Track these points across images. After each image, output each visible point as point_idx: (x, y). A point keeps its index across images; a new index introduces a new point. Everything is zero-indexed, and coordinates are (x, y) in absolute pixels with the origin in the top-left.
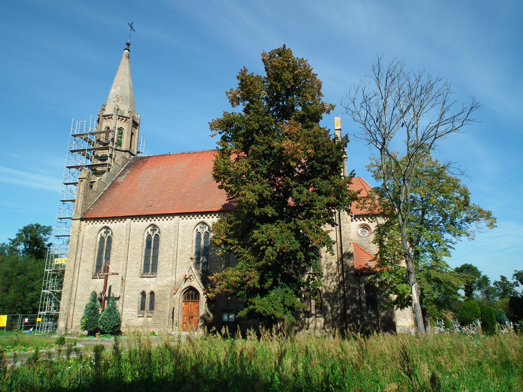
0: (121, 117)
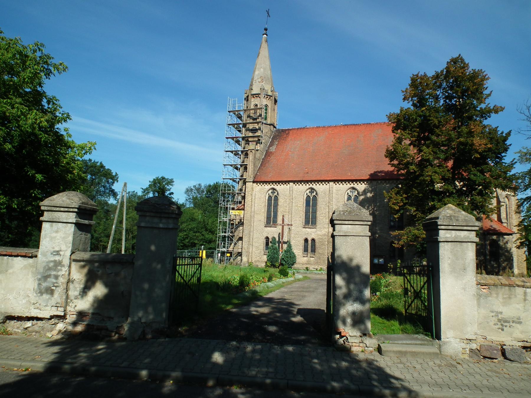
0: (268, 96)
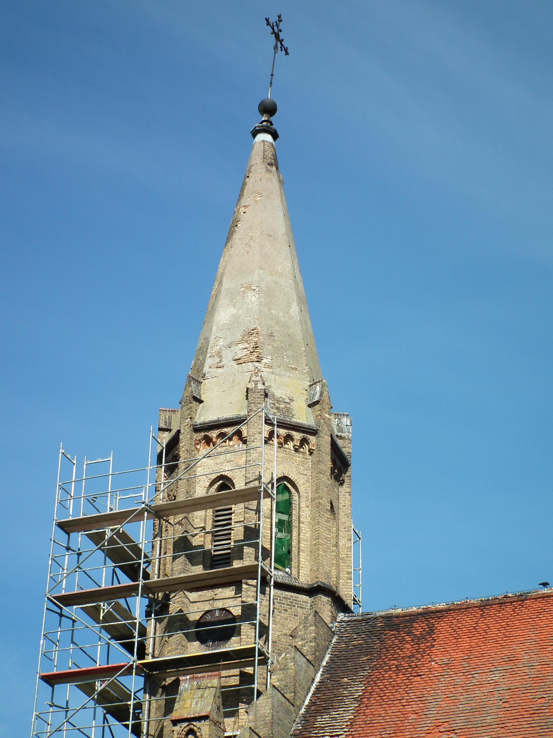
0: (289, 432)
